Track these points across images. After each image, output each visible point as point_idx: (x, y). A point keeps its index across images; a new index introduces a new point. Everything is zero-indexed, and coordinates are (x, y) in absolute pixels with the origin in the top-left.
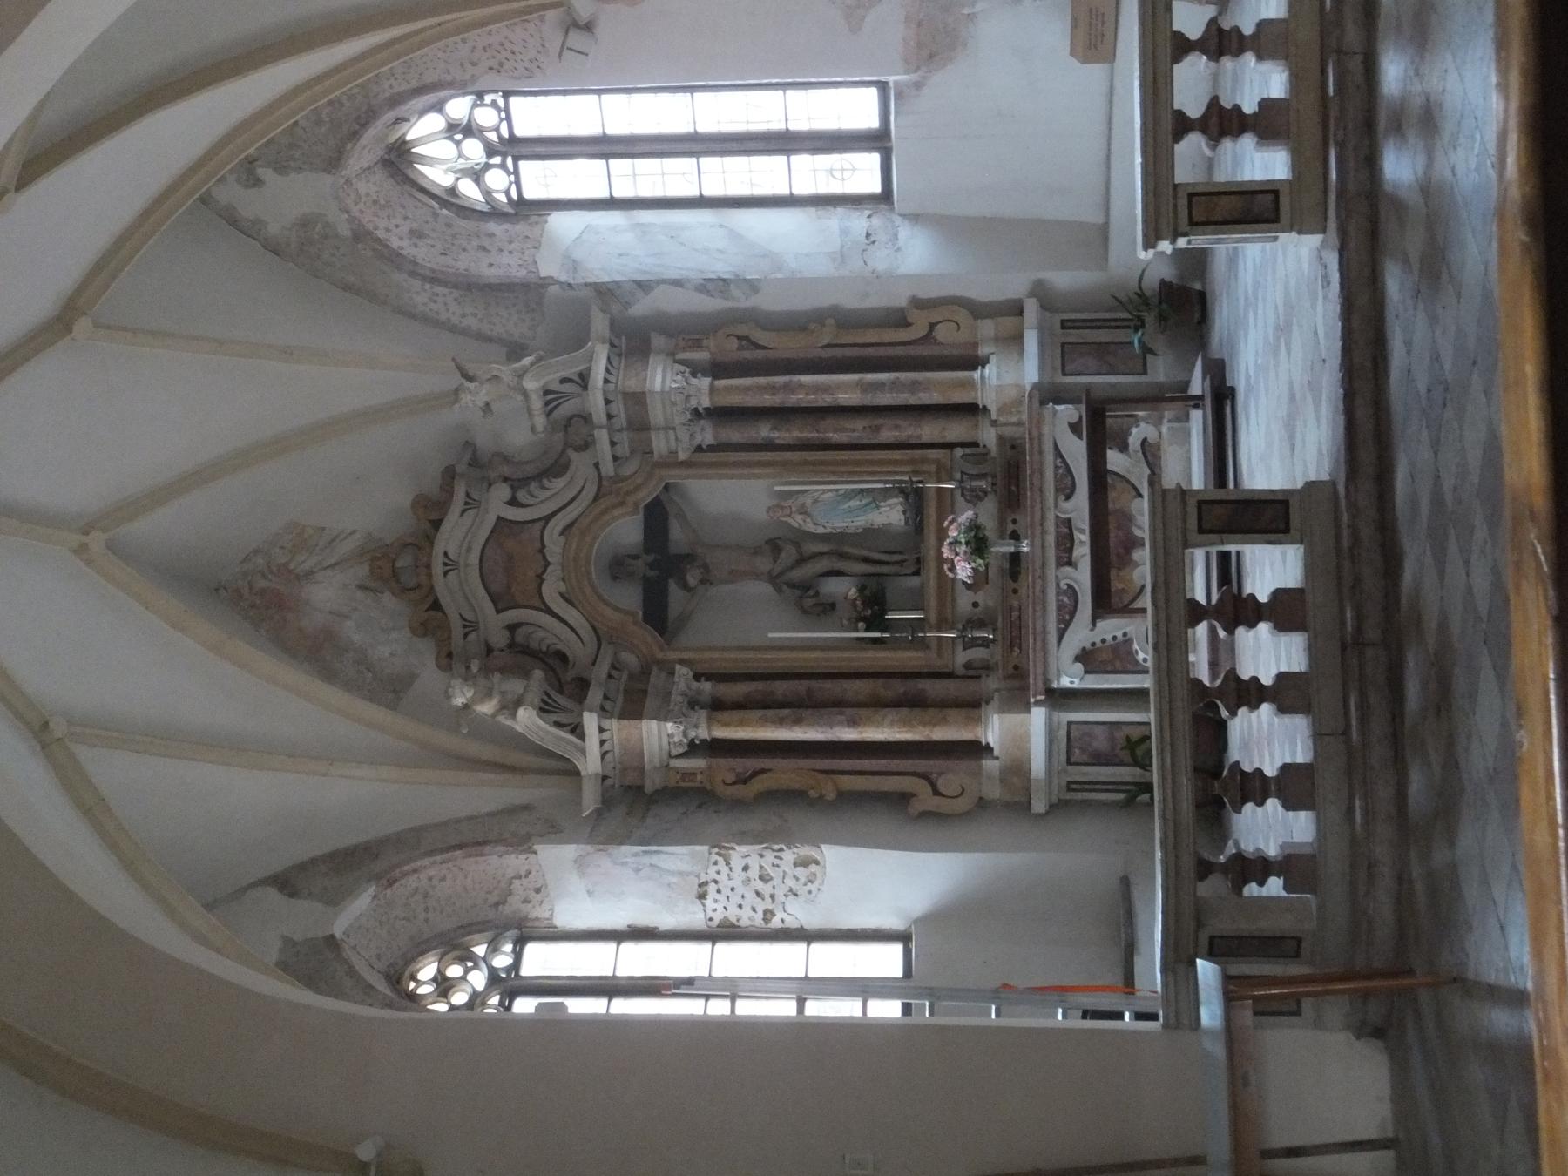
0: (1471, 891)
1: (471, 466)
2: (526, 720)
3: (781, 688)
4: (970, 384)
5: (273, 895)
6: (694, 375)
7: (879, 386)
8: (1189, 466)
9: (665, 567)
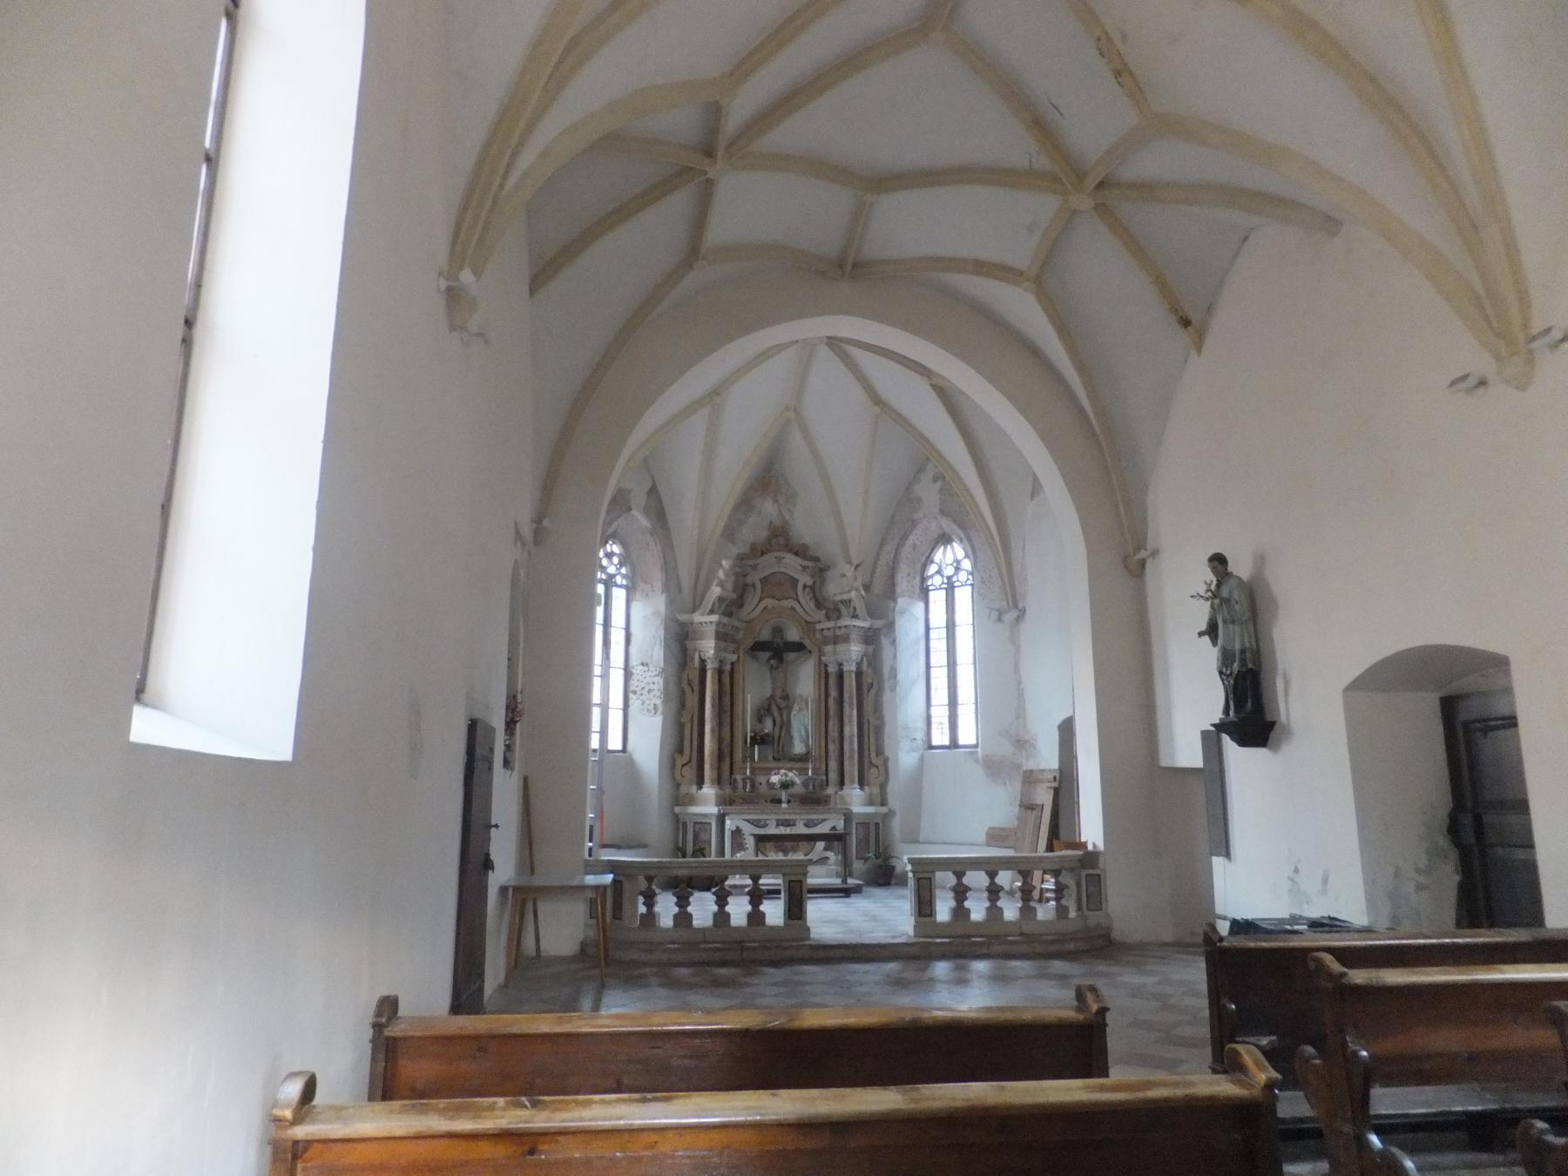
0: (639, 993)
1: (820, 570)
2: (716, 591)
3: (727, 700)
4: (852, 782)
7: (851, 743)
8: (817, 877)
9: (777, 651)
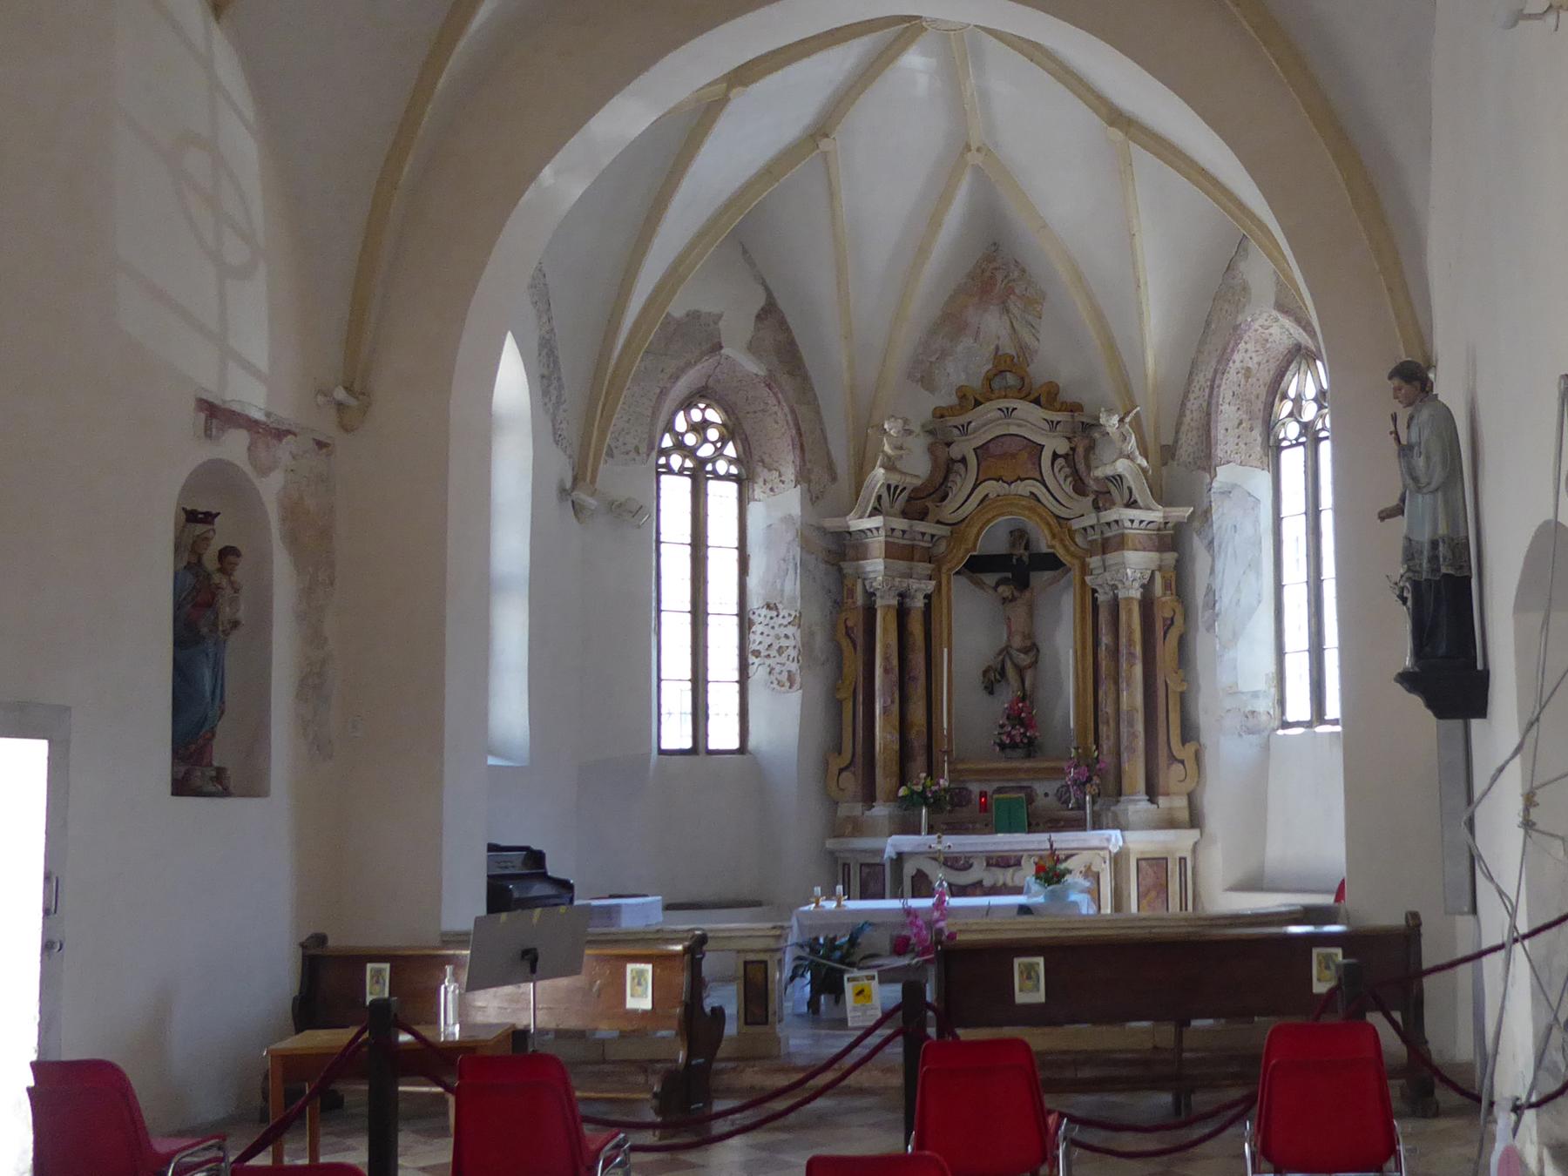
5: (760, 301)
6: (1143, 586)
9: (1016, 569)
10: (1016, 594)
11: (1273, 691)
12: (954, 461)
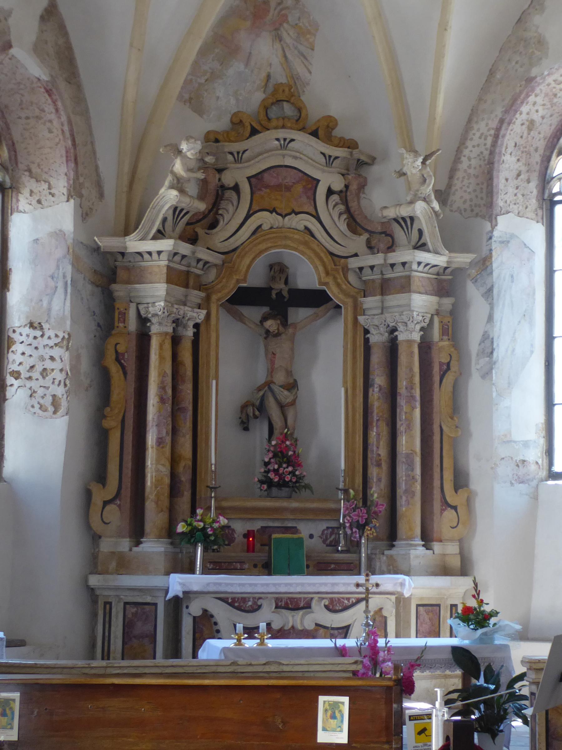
2: (169, 197)
9: (276, 302)
10: (281, 329)
11: (542, 441)
12: (223, 187)
